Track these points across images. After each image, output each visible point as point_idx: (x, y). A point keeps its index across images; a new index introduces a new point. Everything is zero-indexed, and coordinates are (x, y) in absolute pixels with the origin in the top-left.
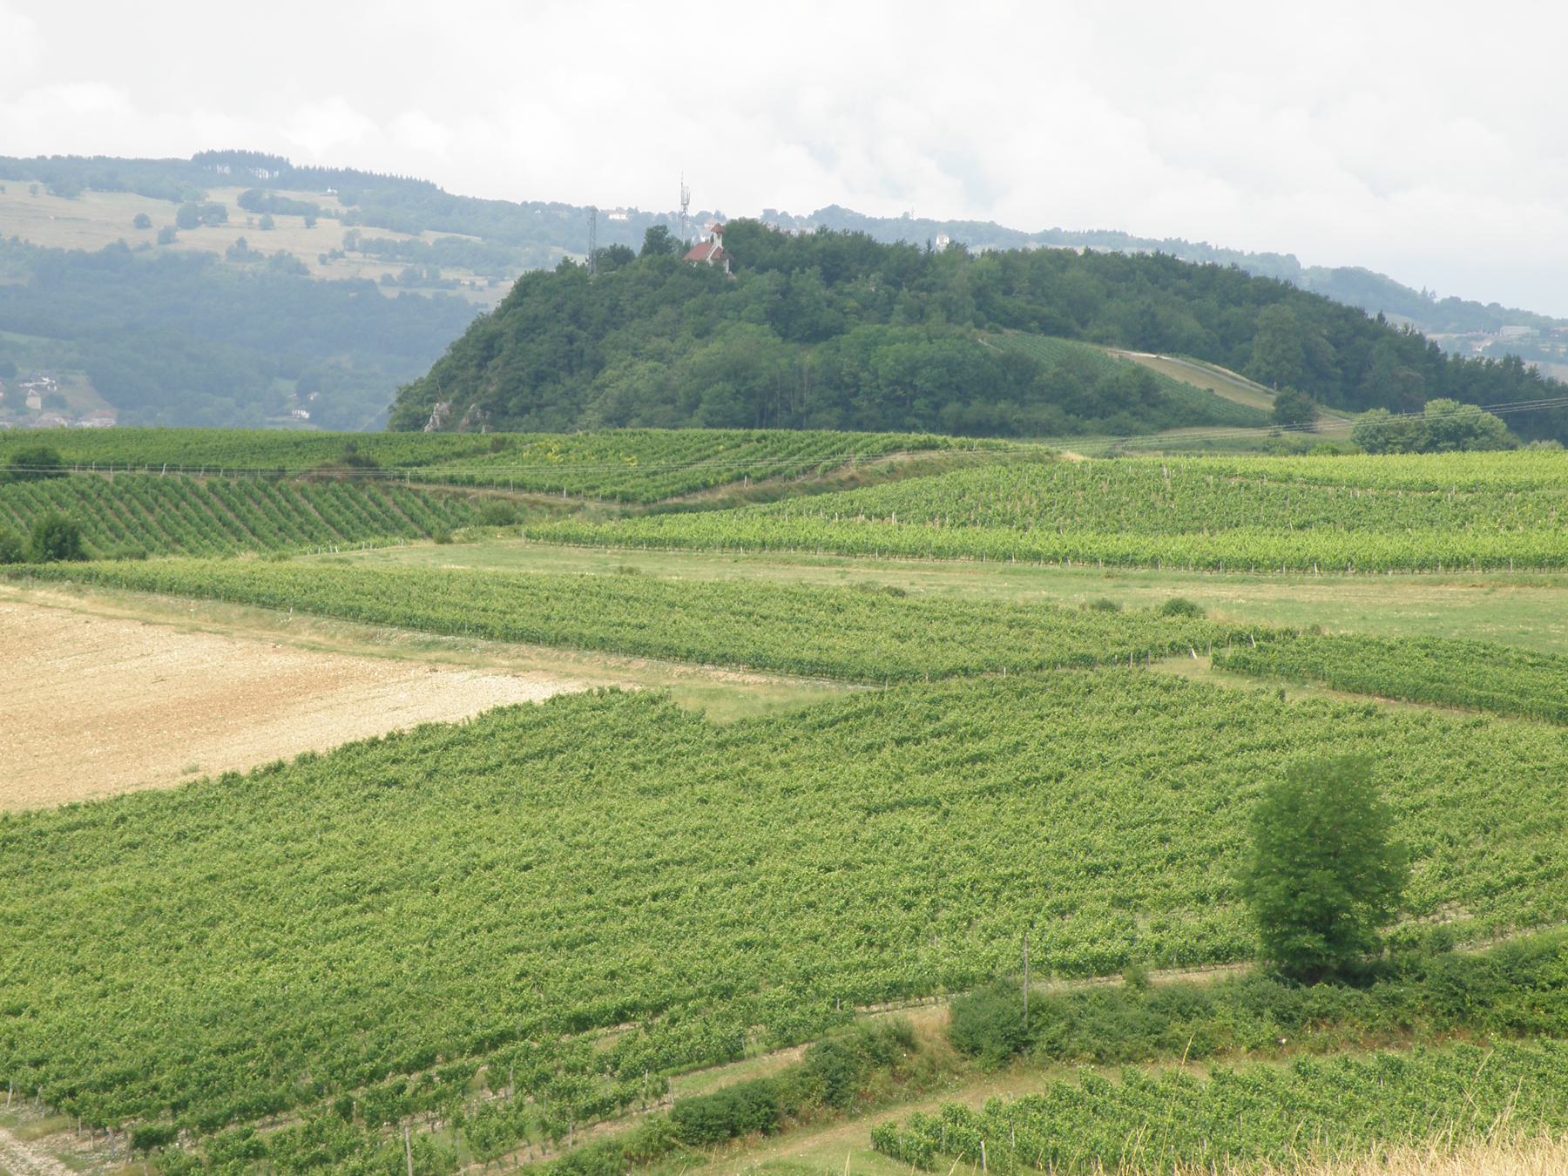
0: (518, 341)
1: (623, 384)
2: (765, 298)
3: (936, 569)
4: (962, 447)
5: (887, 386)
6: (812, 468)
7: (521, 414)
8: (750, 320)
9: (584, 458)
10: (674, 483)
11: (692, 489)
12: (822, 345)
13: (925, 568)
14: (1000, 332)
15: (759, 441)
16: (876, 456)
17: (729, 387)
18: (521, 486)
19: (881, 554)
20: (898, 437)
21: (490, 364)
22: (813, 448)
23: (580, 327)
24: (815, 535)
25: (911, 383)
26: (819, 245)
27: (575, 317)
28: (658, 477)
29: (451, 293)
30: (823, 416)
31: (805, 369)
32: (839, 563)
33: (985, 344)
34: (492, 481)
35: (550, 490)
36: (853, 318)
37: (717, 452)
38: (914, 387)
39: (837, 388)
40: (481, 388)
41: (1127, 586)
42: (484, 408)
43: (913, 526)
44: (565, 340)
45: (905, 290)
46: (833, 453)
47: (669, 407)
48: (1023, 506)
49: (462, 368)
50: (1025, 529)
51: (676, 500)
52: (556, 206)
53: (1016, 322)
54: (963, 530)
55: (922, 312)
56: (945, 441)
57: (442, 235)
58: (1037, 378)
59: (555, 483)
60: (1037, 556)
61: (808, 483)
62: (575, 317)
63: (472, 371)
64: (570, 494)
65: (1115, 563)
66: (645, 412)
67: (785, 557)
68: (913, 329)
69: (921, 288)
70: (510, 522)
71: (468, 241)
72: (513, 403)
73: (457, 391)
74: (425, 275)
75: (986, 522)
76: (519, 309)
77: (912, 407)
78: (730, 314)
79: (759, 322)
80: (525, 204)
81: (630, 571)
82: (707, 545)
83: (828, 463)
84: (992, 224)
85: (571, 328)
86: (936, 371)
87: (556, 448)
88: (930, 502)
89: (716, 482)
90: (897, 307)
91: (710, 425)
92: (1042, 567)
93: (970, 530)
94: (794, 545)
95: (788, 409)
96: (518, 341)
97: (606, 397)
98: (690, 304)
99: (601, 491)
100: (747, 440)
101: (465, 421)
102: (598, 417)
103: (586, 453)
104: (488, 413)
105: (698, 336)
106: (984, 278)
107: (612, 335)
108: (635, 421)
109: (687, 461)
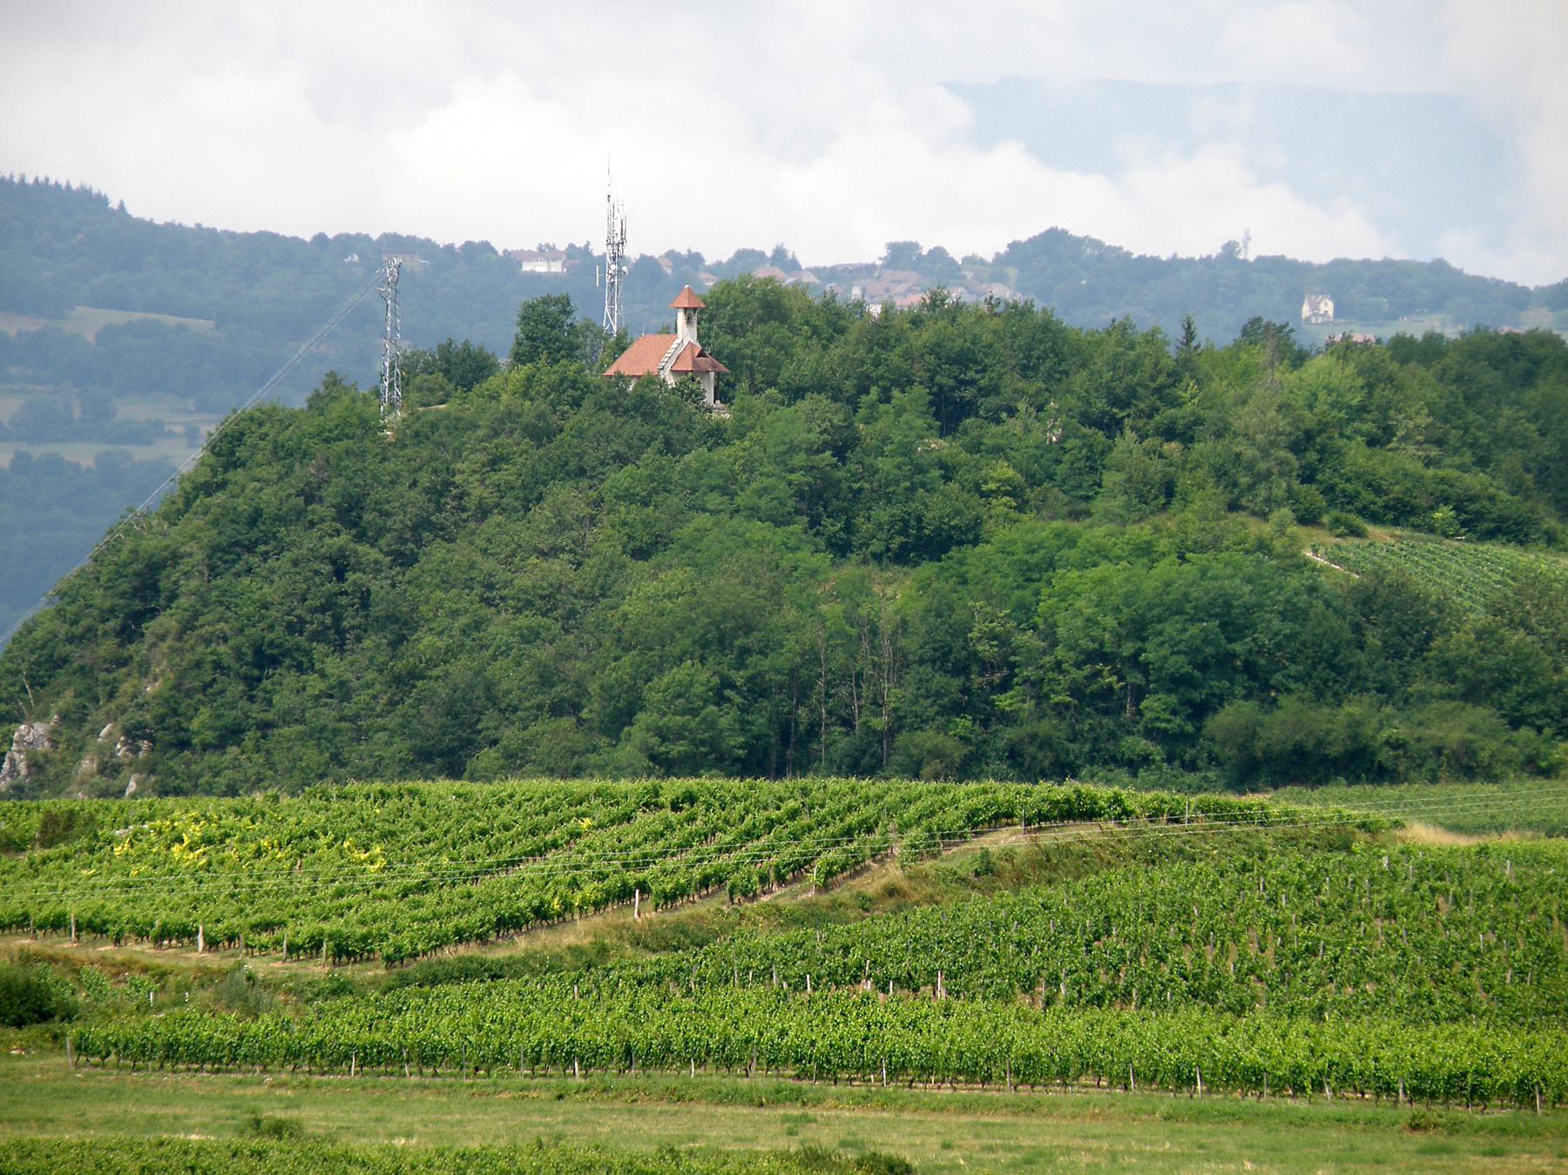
0: (214, 572)
1: (460, 669)
2: (799, 459)
3: (1016, 1109)
4: (1154, 815)
5: (1079, 666)
6: (800, 867)
7: (220, 745)
8: (754, 513)
9: (258, 853)
10: (464, 910)
11: (509, 924)
12: (927, 569)
13: (993, 1107)
14: (1357, 533)
15: (675, 807)
16: (950, 837)
17: (703, 677)
18: (94, 927)
19: (893, 1074)
20: (1007, 791)
21: (152, 627)
22: (805, 820)
23: (360, 537)
24: (748, 1029)
25: (1134, 660)
26: (926, 336)
27: (350, 513)
28: (429, 898)
29: (140, 454)
30: (929, 738)
31: (886, 628)
32: (797, 1097)
33: (1321, 561)
34: (26, 916)
35: (165, 934)
36: (1001, 505)
37: (576, 835)
38: (1144, 668)
39: (961, 670)
40: (126, 687)
41: (1449, 1150)
42: (133, 734)
43: (979, 1005)
44: (327, 568)
45: (1130, 435)
46: (849, 833)
47: (567, 722)
48: (1242, 957)
49: (82, 638)
50: (1239, 1009)
51: (462, 950)
52: (395, 243)
53: (1400, 513)
54: (1094, 1013)
55: (1169, 490)
56: (1117, 800)
57: (118, 317)
58: (1437, 642)
59: (177, 918)
60: (1252, 1078)
61: (786, 903)
62: (350, 513)
63: (107, 647)
64: (212, 944)
65: (1433, 1096)
66: (510, 735)
67: (674, 1084)
68: (1141, 532)
69: (1169, 433)
70: (45, 1016)
71: (181, 328)
72: (200, 723)
73: (69, 694)
74: (77, 413)
75: (1151, 997)
76: (220, 497)
77: (1140, 713)
78: (713, 500)
79: (779, 521)
80: (321, 239)
81: (278, 1129)
82: (499, 1058)
83: (832, 855)
84: (1439, 266)
85: (342, 539)
86: (1193, 630)
87: (195, 831)
88: (1024, 947)
89: (567, 906)
90: (1110, 478)
91: (667, 766)
92: (1268, 1103)
93: (1109, 1016)
94: (699, 1055)
95: (848, 723)
96: (214, 572)
97: (419, 701)
98: (619, 478)
99: (286, 934)
100: (651, 805)
101: (87, 765)
102: (401, 747)
103: (265, 843)
104: (145, 745)
105: (640, 554)
106: (1320, 408)
107: (436, 551)
108: (487, 757)
109: (505, 855)
